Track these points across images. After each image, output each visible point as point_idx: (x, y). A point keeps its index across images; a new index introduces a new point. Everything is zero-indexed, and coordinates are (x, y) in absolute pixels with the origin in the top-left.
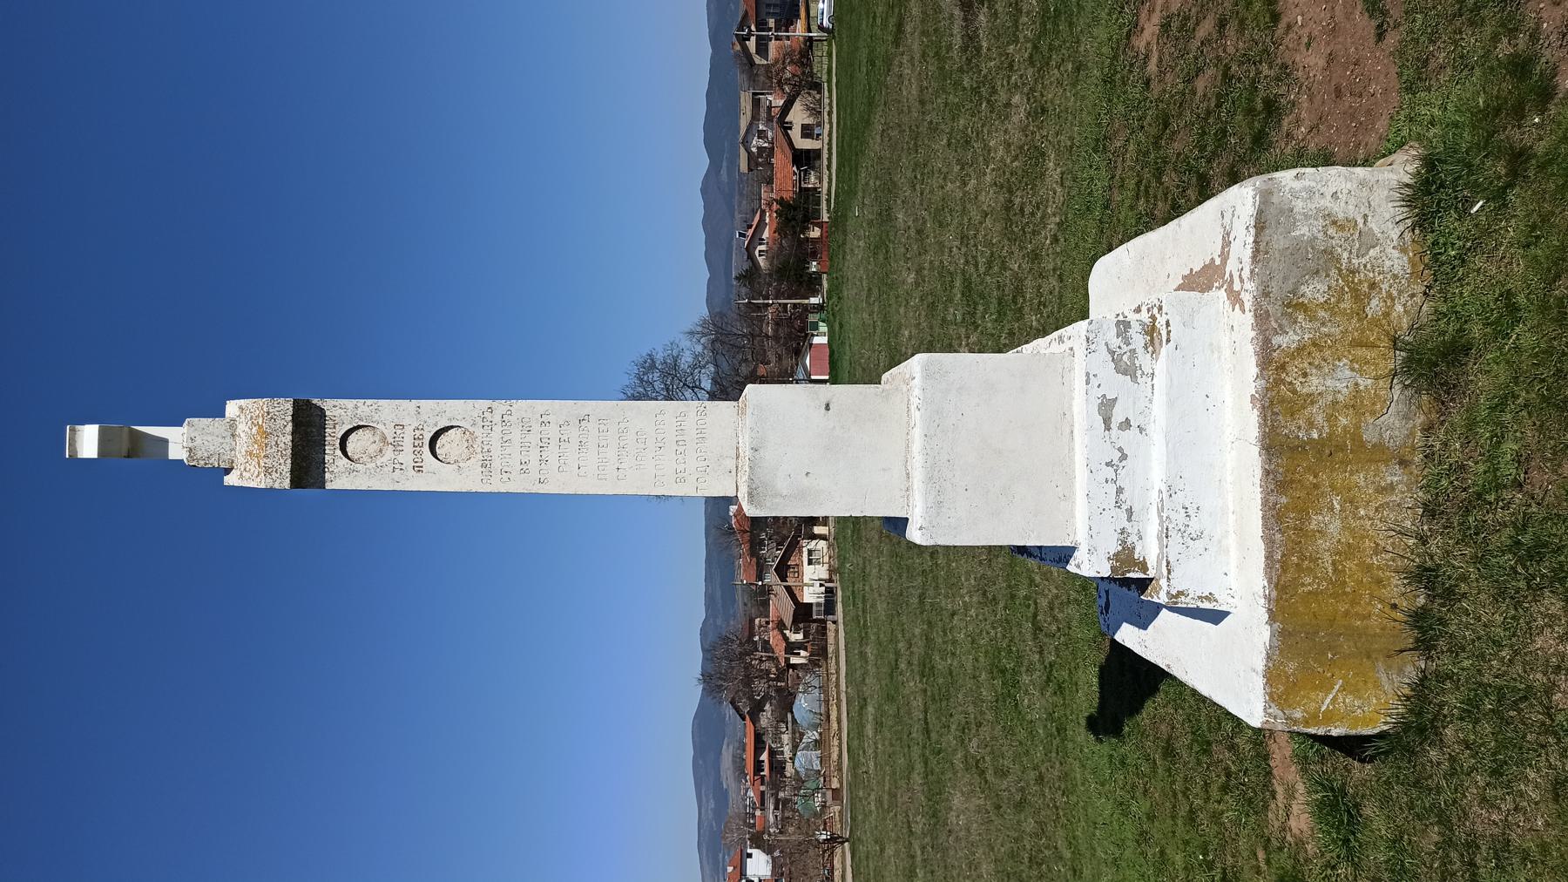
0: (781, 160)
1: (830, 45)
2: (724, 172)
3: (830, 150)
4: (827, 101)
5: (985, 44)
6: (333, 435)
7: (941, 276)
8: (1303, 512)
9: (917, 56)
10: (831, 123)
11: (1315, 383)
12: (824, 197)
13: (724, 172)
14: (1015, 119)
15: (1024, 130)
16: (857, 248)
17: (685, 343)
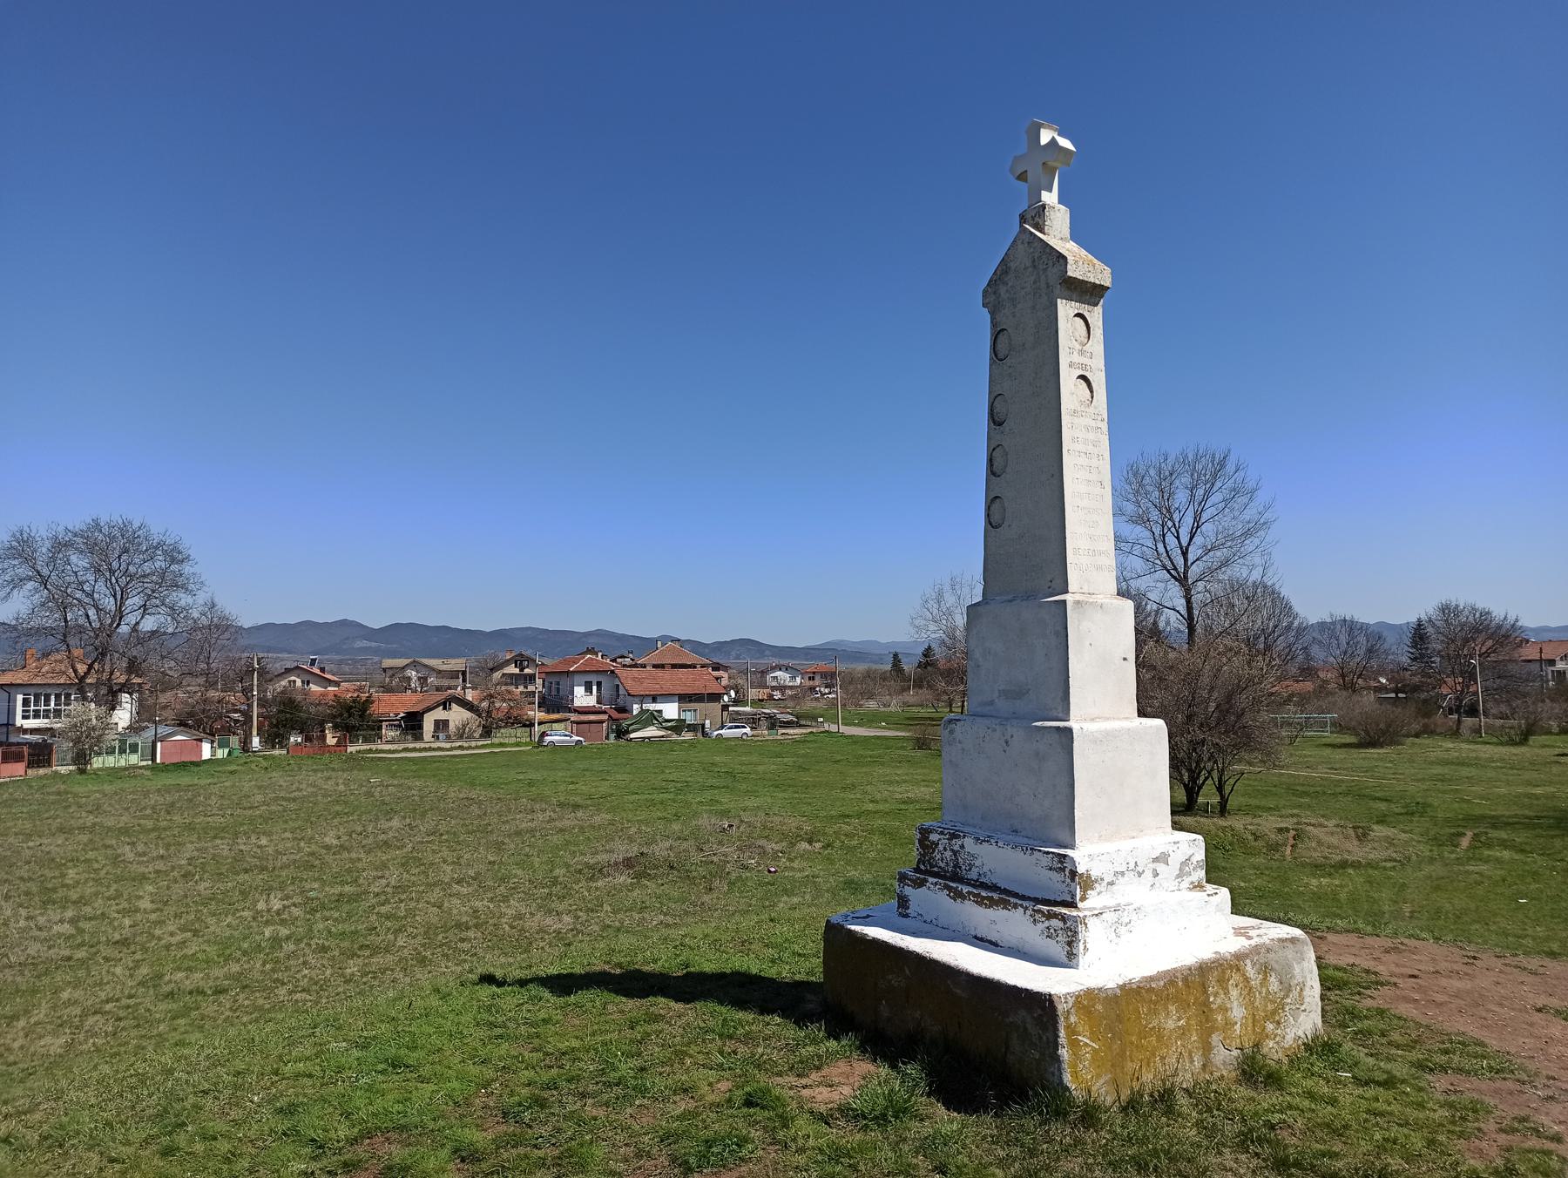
0: (406, 702)
1: (526, 744)
2: (365, 643)
3: (425, 749)
4: (473, 744)
5: (599, 884)
6: (1084, 309)
7: (349, 871)
8: (1176, 999)
9: (559, 824)
10: (451, 749)
11: (1234, 993)
12: (374, 747)
13: (365, 643)
14: (549, 921)
15: (541, 930)
16: (337, 782)
17: (202, 597)
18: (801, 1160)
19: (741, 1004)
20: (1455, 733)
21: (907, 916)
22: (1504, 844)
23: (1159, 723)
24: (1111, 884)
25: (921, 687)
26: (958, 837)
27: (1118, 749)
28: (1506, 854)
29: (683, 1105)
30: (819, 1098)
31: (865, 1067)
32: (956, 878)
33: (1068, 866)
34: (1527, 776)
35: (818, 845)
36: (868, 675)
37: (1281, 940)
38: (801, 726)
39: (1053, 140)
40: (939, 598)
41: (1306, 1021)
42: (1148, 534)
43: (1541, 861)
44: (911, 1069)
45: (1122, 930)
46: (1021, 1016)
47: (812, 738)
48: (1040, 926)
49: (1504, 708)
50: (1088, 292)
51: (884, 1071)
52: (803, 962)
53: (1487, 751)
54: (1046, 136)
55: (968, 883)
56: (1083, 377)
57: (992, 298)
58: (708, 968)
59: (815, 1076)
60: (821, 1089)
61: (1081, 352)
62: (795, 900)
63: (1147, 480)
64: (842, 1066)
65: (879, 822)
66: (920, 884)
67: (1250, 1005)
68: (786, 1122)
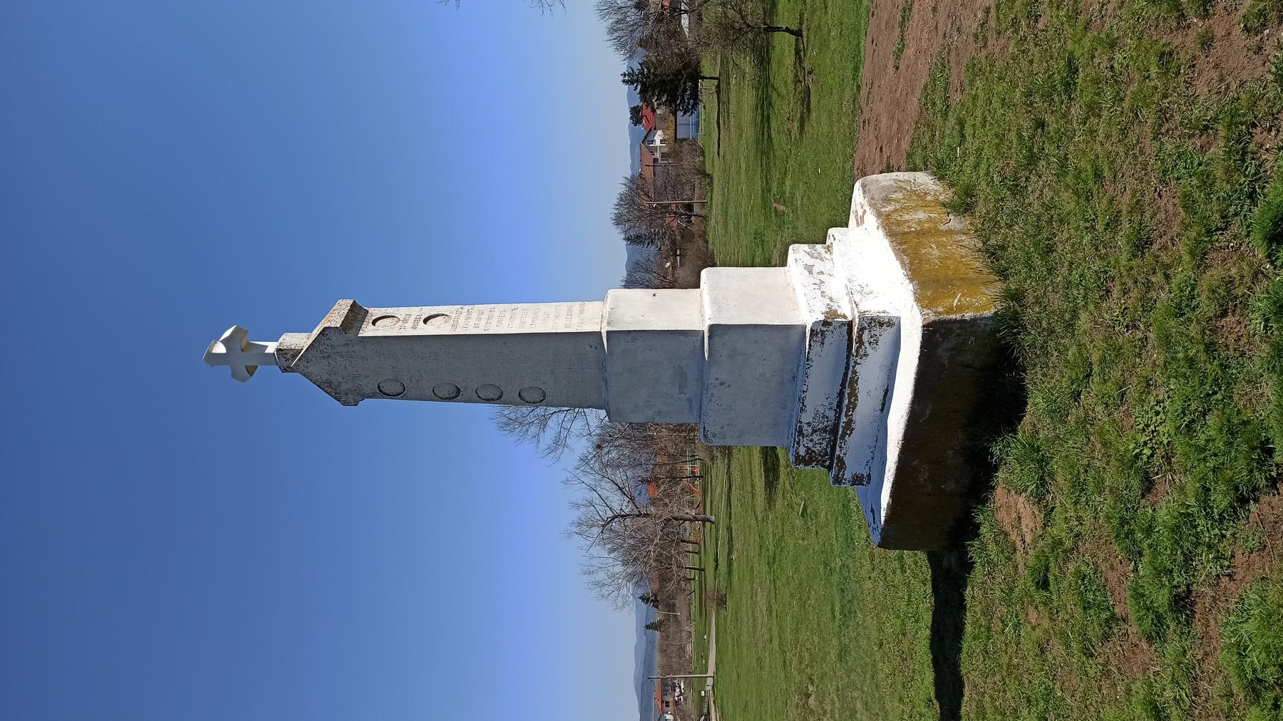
6: (369, 319)
11: (907, 217)
18: (1088, 516)
19: (959, 630)
20: (705, 218)
21: (869, 476)
22: (782, 183)
23: (704, 273)
24: (831, 299)
25: (674, 605)
26: (801, 428)
27: (722, 298)
28: (788, 183)
29: (1057, 648)
30: (1031, 525)
31: (999, 494)
32: (835, 432)
33: (820, 327)
34: (733, 173)
35: (811, 688)
36: (664, 652)
37: (864, 192)
38: (709, 713)
39: (224, 342)
40: (599, 584)
41: (924, 180)
42: (554, 416)
43: (791, 162)
44: (996, 449)
45: (866, 290)
46: (942, 352)
47: (719, 701)
48: (869, 351)
49: (687, 188)
50: (356, 315)
51: (1001, 474)
52: (917, 563)
53: (717, 198)
54: (220, 349)
55: (838, 419)
56: (425, 321)
57: (351, 398)
58: (929, 676)
59: (1014, 536)
60: (1023, 527)
61: (405, 321)
62: (859, 705)
63: (512, 416)
64: (1002, 515)
65: (788, 635)
66: (841, 461)
67: (915, 208)
68: (1057, 543)
